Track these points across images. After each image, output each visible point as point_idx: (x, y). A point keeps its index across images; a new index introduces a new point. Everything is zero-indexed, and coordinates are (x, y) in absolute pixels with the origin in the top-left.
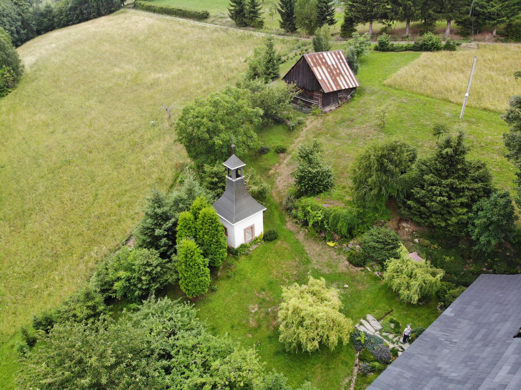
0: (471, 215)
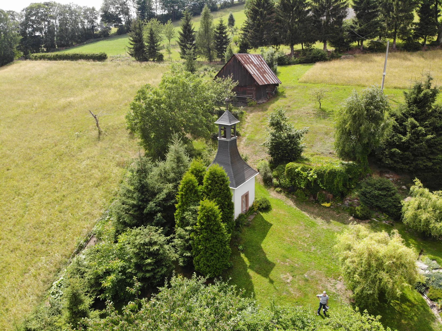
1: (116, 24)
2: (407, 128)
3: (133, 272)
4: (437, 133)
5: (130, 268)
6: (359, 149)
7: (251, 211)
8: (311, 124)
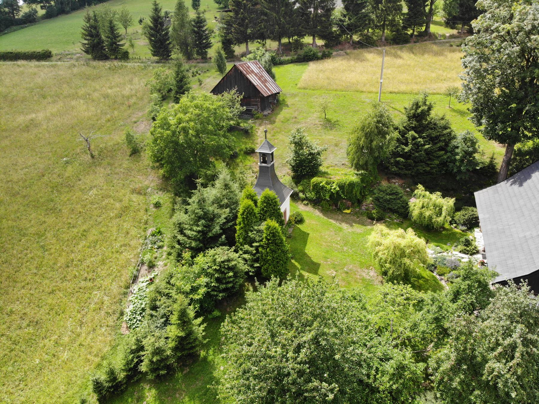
0: (449, 154)
1: (42, 4)
2: (409, 140)
5: (212, 282)
6: (371, 162)
8: (321, 136)
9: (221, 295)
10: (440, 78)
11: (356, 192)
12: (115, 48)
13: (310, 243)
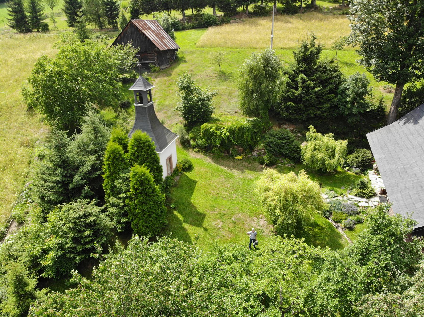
2: (299, 83)
3: (72, 246)
4: (322, 86)
5: (67, 243)
6: (262, 106)
7: (175, 172)
8: (215, 87)
9: (78, 258)
10: (327, 37)
11: (247, 137)
12: (37, 22)
13: (197, 191)
